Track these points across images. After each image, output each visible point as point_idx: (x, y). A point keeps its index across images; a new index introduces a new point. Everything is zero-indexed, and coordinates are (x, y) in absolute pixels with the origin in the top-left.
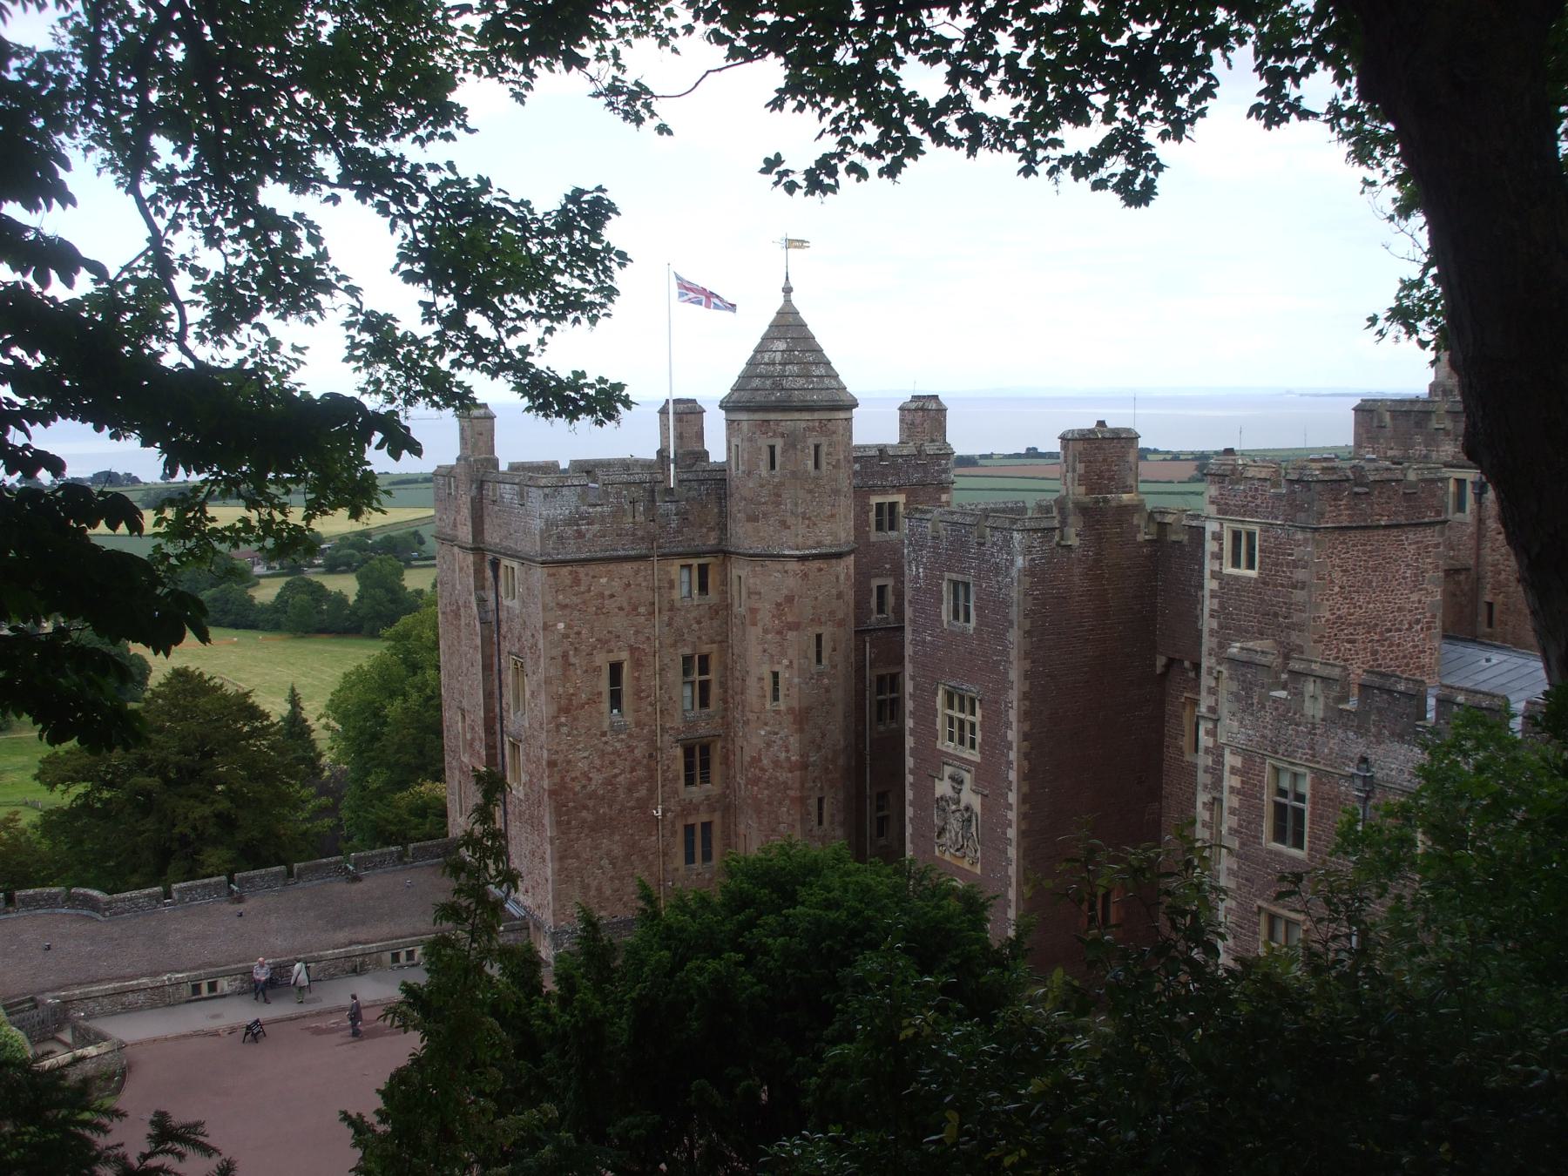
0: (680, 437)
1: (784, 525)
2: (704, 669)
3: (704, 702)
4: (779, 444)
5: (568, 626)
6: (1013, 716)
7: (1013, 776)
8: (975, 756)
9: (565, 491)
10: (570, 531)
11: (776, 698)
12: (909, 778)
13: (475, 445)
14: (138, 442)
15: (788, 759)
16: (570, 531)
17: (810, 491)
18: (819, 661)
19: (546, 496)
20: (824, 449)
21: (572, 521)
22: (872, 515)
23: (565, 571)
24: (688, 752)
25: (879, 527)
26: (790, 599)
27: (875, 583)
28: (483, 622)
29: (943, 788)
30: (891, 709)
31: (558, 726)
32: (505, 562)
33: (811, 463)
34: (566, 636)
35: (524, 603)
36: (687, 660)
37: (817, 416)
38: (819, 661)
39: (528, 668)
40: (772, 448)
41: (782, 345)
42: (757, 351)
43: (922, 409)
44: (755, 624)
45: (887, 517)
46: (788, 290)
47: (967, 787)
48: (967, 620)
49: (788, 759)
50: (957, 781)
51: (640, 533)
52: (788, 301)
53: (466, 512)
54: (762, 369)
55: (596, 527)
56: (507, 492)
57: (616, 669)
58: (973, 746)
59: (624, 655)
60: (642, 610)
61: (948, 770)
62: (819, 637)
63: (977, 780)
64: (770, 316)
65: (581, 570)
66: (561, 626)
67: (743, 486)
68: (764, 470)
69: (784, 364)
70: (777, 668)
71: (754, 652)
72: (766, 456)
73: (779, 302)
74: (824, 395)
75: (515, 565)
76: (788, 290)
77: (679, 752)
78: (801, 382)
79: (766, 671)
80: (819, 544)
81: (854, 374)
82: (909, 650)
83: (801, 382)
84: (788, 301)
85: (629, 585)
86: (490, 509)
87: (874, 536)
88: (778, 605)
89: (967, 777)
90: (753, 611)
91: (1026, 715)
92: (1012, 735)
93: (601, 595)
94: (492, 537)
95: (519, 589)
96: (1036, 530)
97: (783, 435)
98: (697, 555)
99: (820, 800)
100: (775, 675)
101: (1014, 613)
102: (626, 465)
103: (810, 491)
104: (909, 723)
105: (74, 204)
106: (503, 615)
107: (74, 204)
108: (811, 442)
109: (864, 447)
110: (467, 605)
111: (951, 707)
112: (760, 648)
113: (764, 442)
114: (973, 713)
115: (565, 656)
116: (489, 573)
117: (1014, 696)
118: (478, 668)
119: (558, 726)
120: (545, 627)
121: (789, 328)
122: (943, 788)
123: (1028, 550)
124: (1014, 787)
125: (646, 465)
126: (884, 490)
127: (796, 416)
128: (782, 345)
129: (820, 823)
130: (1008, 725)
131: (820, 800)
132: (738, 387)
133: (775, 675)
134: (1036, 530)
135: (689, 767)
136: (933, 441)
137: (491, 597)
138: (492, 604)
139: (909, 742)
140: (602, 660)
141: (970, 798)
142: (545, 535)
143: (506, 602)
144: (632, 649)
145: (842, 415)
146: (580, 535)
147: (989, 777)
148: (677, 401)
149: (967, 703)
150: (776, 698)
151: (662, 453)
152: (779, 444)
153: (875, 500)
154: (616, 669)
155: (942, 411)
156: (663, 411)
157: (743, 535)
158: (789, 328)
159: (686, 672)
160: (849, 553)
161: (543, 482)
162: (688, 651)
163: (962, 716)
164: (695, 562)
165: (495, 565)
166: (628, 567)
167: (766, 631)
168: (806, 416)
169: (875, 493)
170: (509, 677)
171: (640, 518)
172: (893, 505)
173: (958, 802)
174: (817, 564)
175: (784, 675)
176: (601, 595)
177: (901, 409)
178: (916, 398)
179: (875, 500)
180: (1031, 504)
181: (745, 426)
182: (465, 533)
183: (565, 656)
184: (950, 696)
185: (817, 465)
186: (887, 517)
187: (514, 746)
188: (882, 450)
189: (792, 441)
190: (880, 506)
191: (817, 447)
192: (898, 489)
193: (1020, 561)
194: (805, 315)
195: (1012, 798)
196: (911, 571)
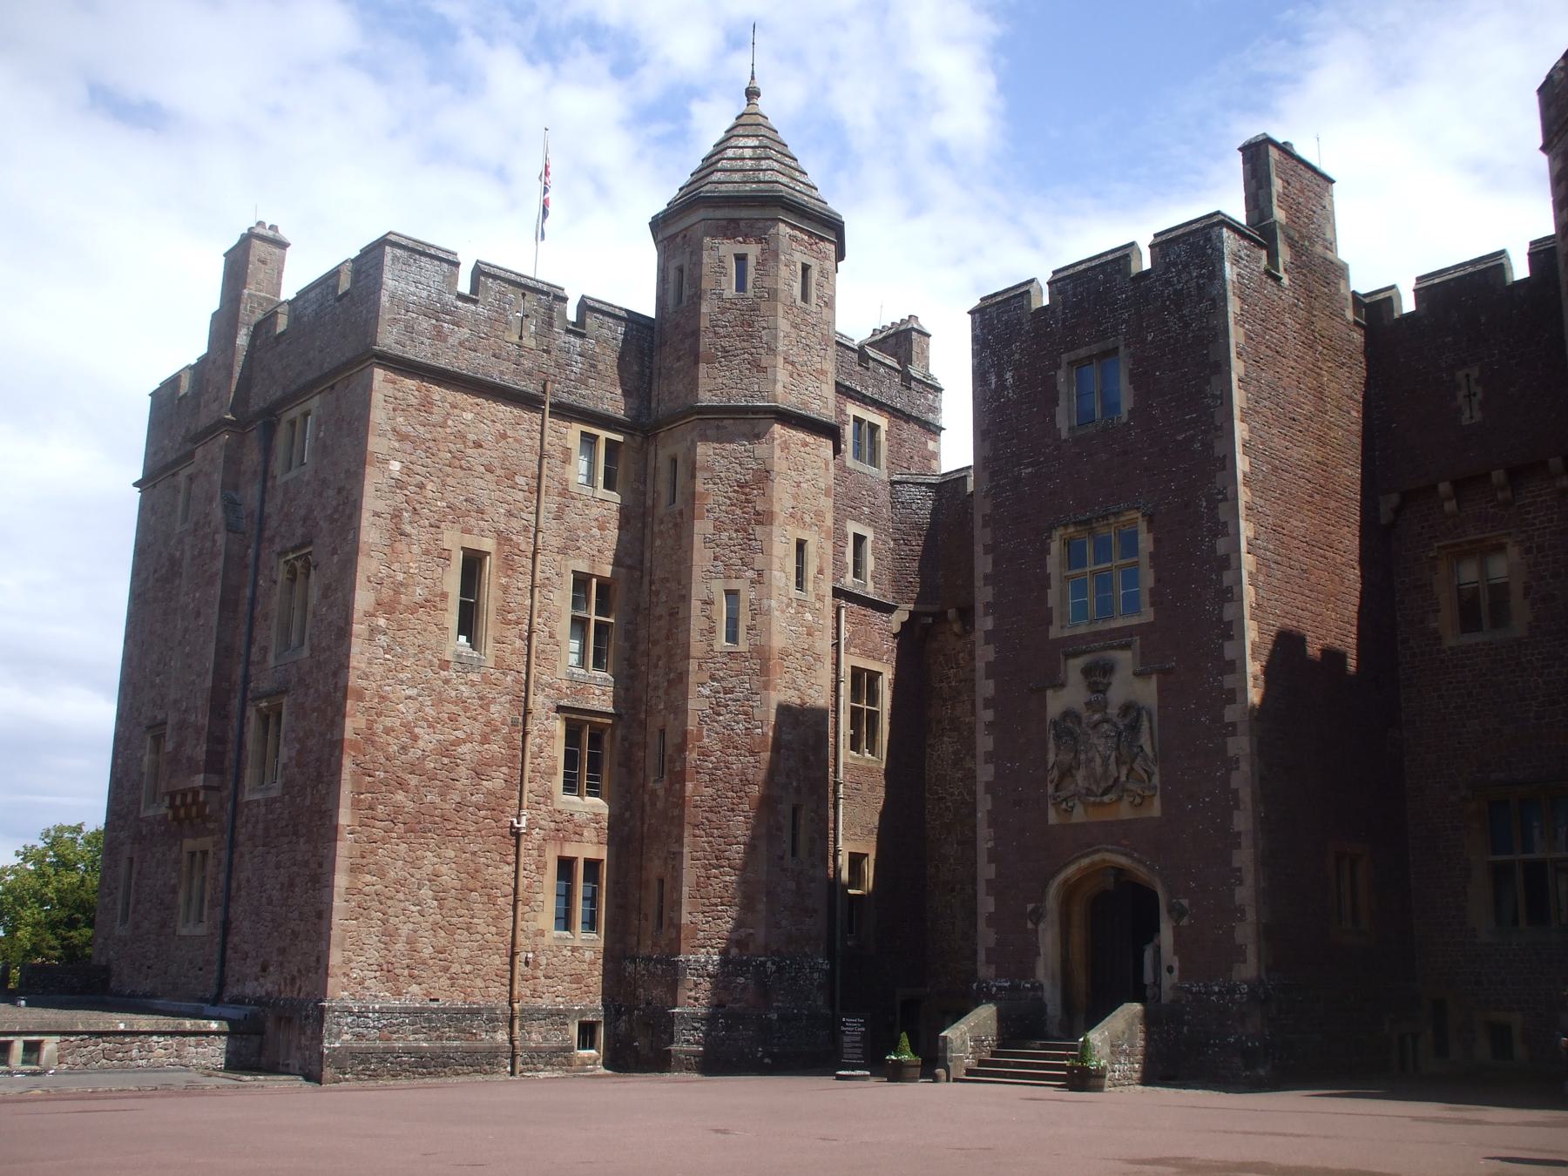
46: (752, 94)
70: (735, 585)
71: (701, 557)
112: (709, 554)
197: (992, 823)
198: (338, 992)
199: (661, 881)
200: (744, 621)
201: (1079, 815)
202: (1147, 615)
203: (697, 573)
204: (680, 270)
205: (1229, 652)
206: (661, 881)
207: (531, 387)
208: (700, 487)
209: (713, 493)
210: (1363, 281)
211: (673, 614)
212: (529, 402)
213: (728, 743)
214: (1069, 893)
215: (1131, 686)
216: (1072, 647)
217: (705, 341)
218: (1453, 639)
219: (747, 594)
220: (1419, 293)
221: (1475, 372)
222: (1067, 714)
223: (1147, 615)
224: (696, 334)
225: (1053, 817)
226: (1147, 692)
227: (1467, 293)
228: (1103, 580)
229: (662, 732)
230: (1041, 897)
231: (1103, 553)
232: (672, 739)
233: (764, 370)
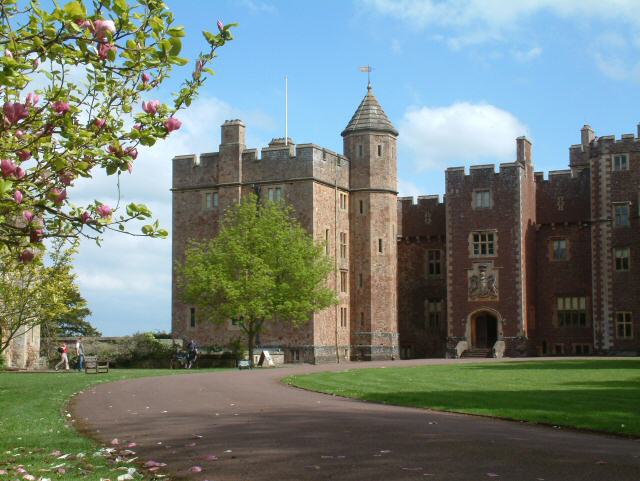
46: (369, 88)
71: (372, 230)
100: (380, 240)
197: (451, 300)
198: (317, 342)
199: (362, 314)
200: (383, 248)
201: (477, 300)
202: (495, 255)
203: (372, 235)
204: (361, 147)
205: (517, 265)
206: (362, 314)
207: (333, 183)
208: (372, 210)
209: (375, 212)
210: (537, 169)
211: (364, 244)
212: (333, 186)
213: (381, 278)
214: (472, 317)
215: (492, 271)
216: (476, 261)
217: (371, 170)
218: (551, 260)
219: (384, 240)
220: (550, 176)
221: (562, 198)
222: (474, 276)
223: (495, 255)
224: (368, 167)
225: (469, 300)
226: (496, 274)
227: (556, 177)
228: (483, 246)
229: (361, 275)
230: (466, 318)
231: (483, 239)
232: (365, 278)
233: (385, 179)
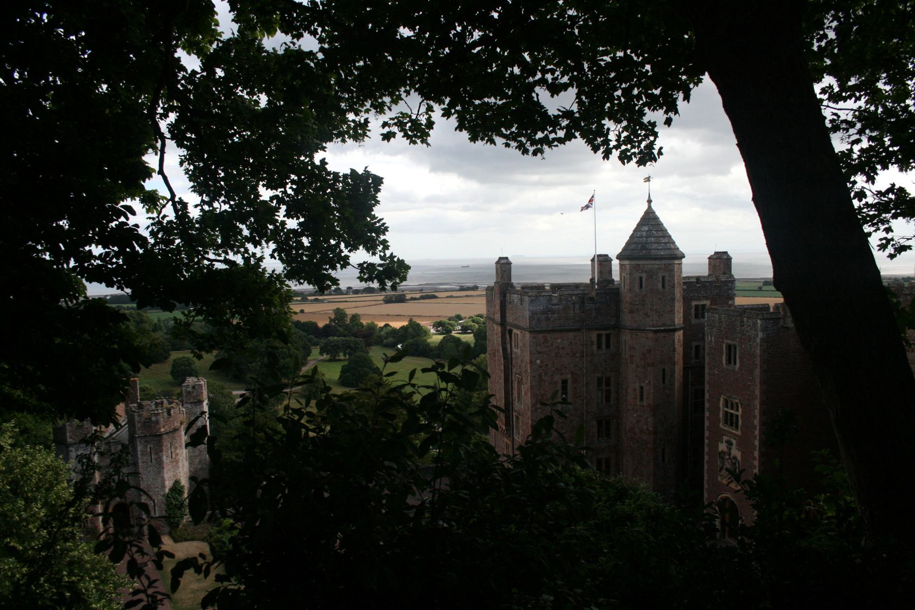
0: (600, 273)
1: (647, 315)
2: (608, 384)
3: (608, 399)
4: (644, 276)
5: (542, 362)
6: (757, 412)
7: (757, 443)
8: (739, 433)
9: (541, 298)
10: (543, 317)
11: (642, 399)
12: (706, 441)
13: (502, 277)
14: (897, 169)
15: (647, 429)
16: (543, 317)
17: (660, 299)
18: (664, 381)
19: (532, 301)
20: (667, 278)
21: (543, 312)
22: (693, 311)
23: (541, 336)
24: (600, 423)
25: (696, 316)
26: (649, 351)
27: (694, 344)
28: (505, 358)
29: (722, 447)
30: (699, 407)
31: (536, 410)
32: (515, 331)
33: (660, 285)
34: (541, 367)
35: (522, 351)
36: (600, 380)
37: (663, 262)
38: (664, 381)
39: (524, 380)
40: (641, 278)
41: (646, 228)
42: (634, 231)
43: (719, 258)
44: (632, 363)
45: (700, 311)
46: (650, 201)
47: (734, 447)
48: (735, 364)
49: (647, 429)
50: (729, 443)
51: (577, 318)
52: (650, 207)
53: (498, 307)
54: (636, 240)
55: (556, 315)
56: (515, 297)
57: (565, 382)
58: (737, 427)
59: (569, 376)
60: (578, 355)
61: (725, 438)
62: (664, 370)
63: (738, 445)
64: (642, 214)
65: (549, 336)
66: (538, 362)
67: (626, 296)
68: (637, 289)
69: (647, 237)
70: (643, 385)
72: (637, 282)
73: (646, 207)
74: (667, 252)
75: (518, 332)
76: (650, 201)
77: (595, 423)
78: (655, 246)
79: (637, 386)
80: (664, 325)
81: (682, 242)
82: (707, 378)
83: (655, 246)
84: (650, 207)
85: (571, 343)
86: (509, 306)
87: (694, 321)
88: (644, 354)
89: (734, 442)
90: (631, 357)
91: (763, 413)
92: (756, 422)
93: (558, 347)
94: (510, 319)
95: (520, 344)
96: (770, 319)
97: (646, 272)
98: (605, 329)
99: (663, 450)
100: (642, 388)
101: (758, 361)
102: (577, 286)
103: (660, 299)
104: (707, 414)
105: (688, 102)
106: (513, 356)
107: (688, 102)
108: (660, 275)
109: (688, 278)
110: (498, 351)
111: (727, 407)
113: (637, 275)
114: (738, 410)
115: (540, 376)
116: (508, 336)
117: (757, 403)
118: (502, 381)
119: (536, 410)
120: (531, 362)
121: (650, 220)
122: (722, 447)
123: (764, 329)
124: (757, 449)
125: (585, 285)
126: (699, 299)
127: (653, 262)
128: (646, 228)
129: (663, 460)
130: (755, 417)
131: (663, 450)
132: (624, 249)
133: (642, 388)
134: (770, 319)
135: (599, 432)
136: (724, 274)
137: (509, 346)
138: (509, 351)
139: (707, 423)
140: (558, 378)
141: (736, 453)
142: (531, 319)
143: (515, 350)
144: (573, 373)
145: (676, 262)
146: (548, 319)
147: (744, 444)
148: (599, 256)
149: (735, 406)
150: (642, 399)
151: (592, 280)
152: (644, 276)
153: (694, 303)
154: (565, 382)
155: (729, 259)
156: (593, 260)
157: (627, 319)
158: (650, 220)
159: (599, 385)
160: (679, 329)
161: (530, 294)
162: (599, 375)
163: (732, 412)
164: (604, 332)
165: (510, 332)
166: (571, 335)
167: (637, 366)
168: (658, 262)
169: (695, 300)
170: (515, 385)
171: (577, 311)
172: (704, 306)
173: (730, 454)
174: (662, 335)
175: (646, 388)
176: (558, 347)
177: (709, 258)
178: (716, 253)
179: (694, 303)
180: (772, 305)
181: (628, 267)
182: (498, 317)
183: (540, 376)
184: (726, 402)
185: (663, 286)
186: (700, 311)
187: (517, 417)
188: (698, 279)
189: (651, 274)
190: (697, 306)
191: (663, 278)
192: (707, 298)
193: (760, 335)
194: (658, 214)
195: (756, 454)
196: (708, 338)
